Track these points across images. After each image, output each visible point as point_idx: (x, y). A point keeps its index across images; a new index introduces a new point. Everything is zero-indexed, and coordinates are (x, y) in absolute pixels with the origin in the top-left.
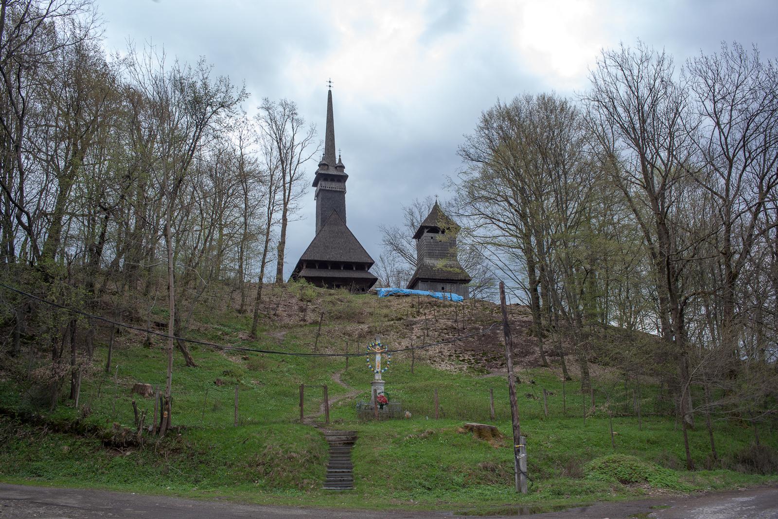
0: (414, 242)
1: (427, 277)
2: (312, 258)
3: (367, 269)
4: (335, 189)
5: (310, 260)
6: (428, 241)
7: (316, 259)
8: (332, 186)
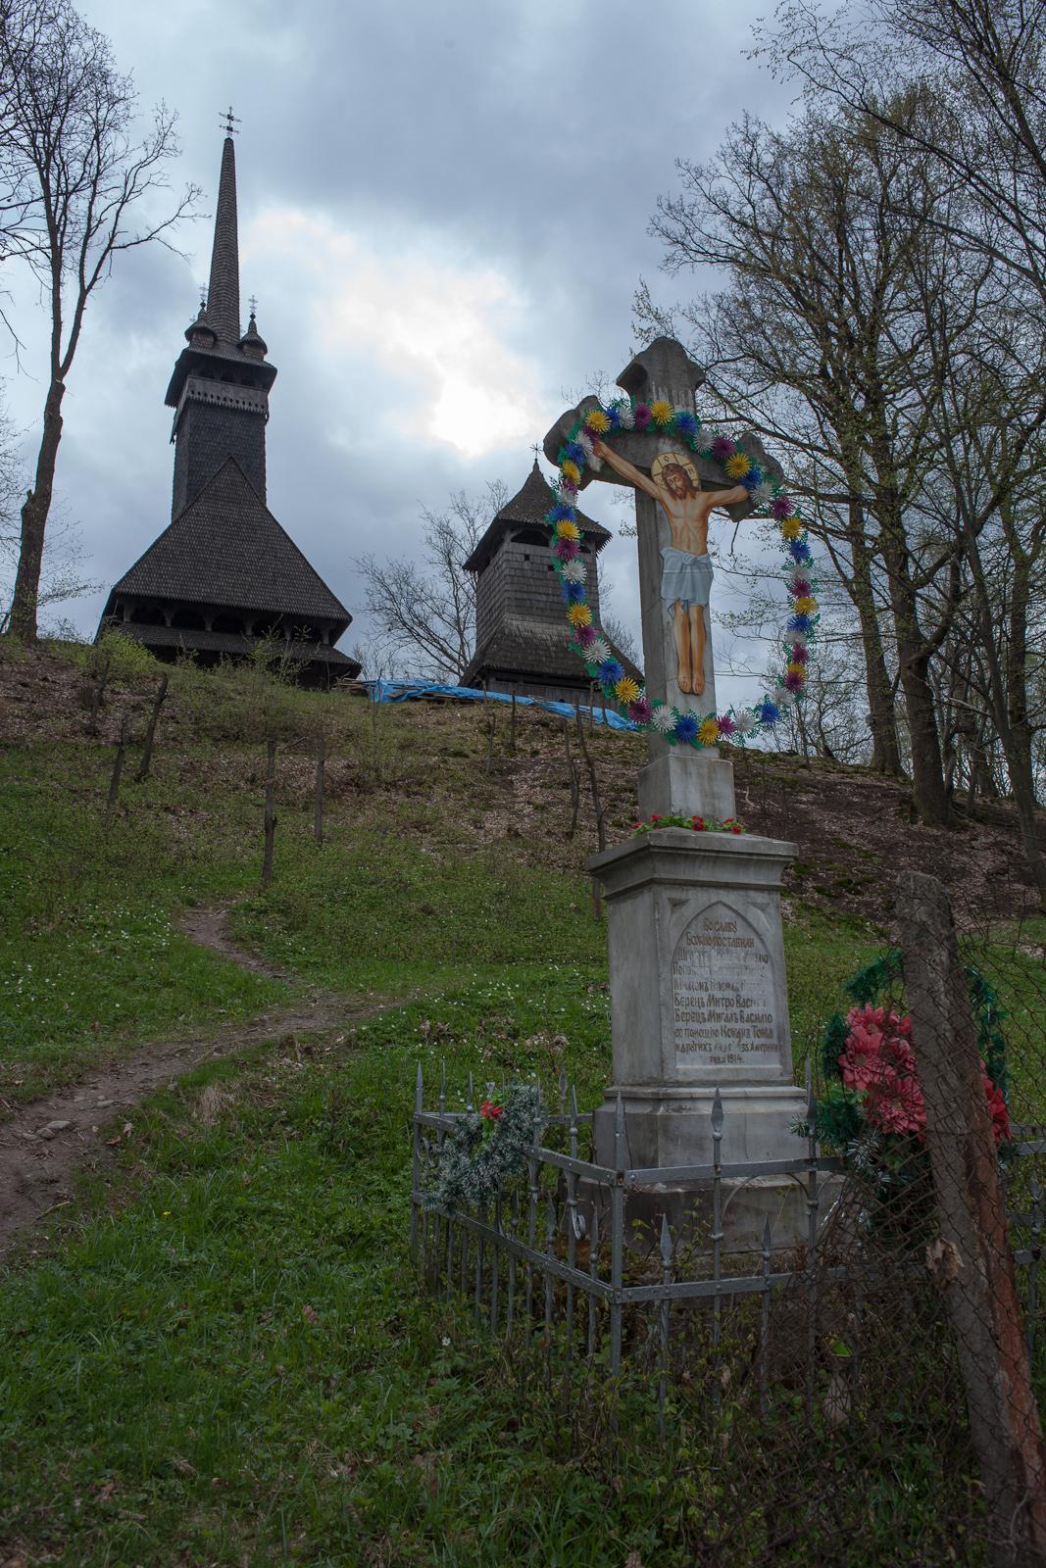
0: (466, 580)
1: (515, 666)
2: (151, 591)
3: (326, 641)
4: (234, 404)
5: (147, 597)
6: (516, 565)
7: (164, 594)
8: (224, 394)
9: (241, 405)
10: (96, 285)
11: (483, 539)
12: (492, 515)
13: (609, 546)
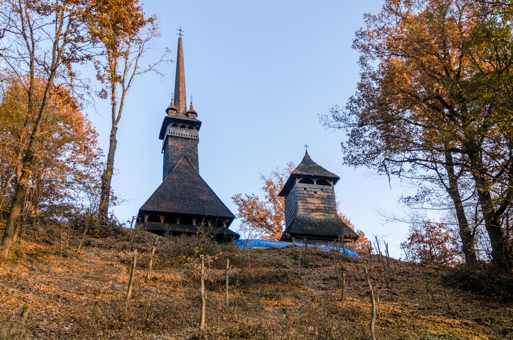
3: (225, 226)
9: (188, 136)
10: (129, 88)
11: (286, 184)
12: (289, 175)
13: (339, 183)
